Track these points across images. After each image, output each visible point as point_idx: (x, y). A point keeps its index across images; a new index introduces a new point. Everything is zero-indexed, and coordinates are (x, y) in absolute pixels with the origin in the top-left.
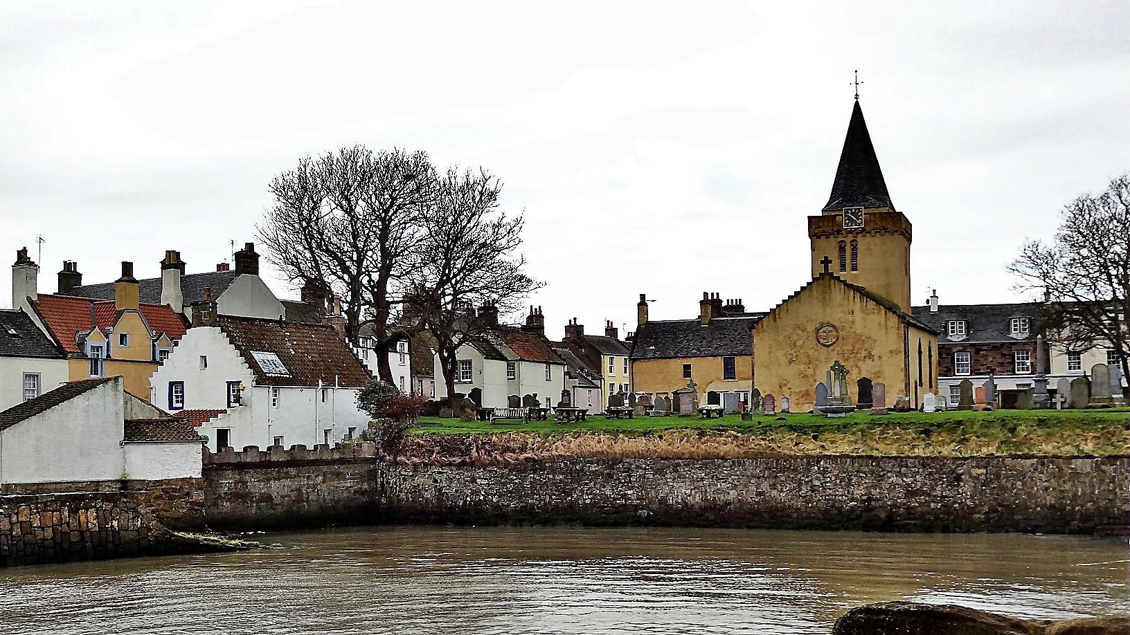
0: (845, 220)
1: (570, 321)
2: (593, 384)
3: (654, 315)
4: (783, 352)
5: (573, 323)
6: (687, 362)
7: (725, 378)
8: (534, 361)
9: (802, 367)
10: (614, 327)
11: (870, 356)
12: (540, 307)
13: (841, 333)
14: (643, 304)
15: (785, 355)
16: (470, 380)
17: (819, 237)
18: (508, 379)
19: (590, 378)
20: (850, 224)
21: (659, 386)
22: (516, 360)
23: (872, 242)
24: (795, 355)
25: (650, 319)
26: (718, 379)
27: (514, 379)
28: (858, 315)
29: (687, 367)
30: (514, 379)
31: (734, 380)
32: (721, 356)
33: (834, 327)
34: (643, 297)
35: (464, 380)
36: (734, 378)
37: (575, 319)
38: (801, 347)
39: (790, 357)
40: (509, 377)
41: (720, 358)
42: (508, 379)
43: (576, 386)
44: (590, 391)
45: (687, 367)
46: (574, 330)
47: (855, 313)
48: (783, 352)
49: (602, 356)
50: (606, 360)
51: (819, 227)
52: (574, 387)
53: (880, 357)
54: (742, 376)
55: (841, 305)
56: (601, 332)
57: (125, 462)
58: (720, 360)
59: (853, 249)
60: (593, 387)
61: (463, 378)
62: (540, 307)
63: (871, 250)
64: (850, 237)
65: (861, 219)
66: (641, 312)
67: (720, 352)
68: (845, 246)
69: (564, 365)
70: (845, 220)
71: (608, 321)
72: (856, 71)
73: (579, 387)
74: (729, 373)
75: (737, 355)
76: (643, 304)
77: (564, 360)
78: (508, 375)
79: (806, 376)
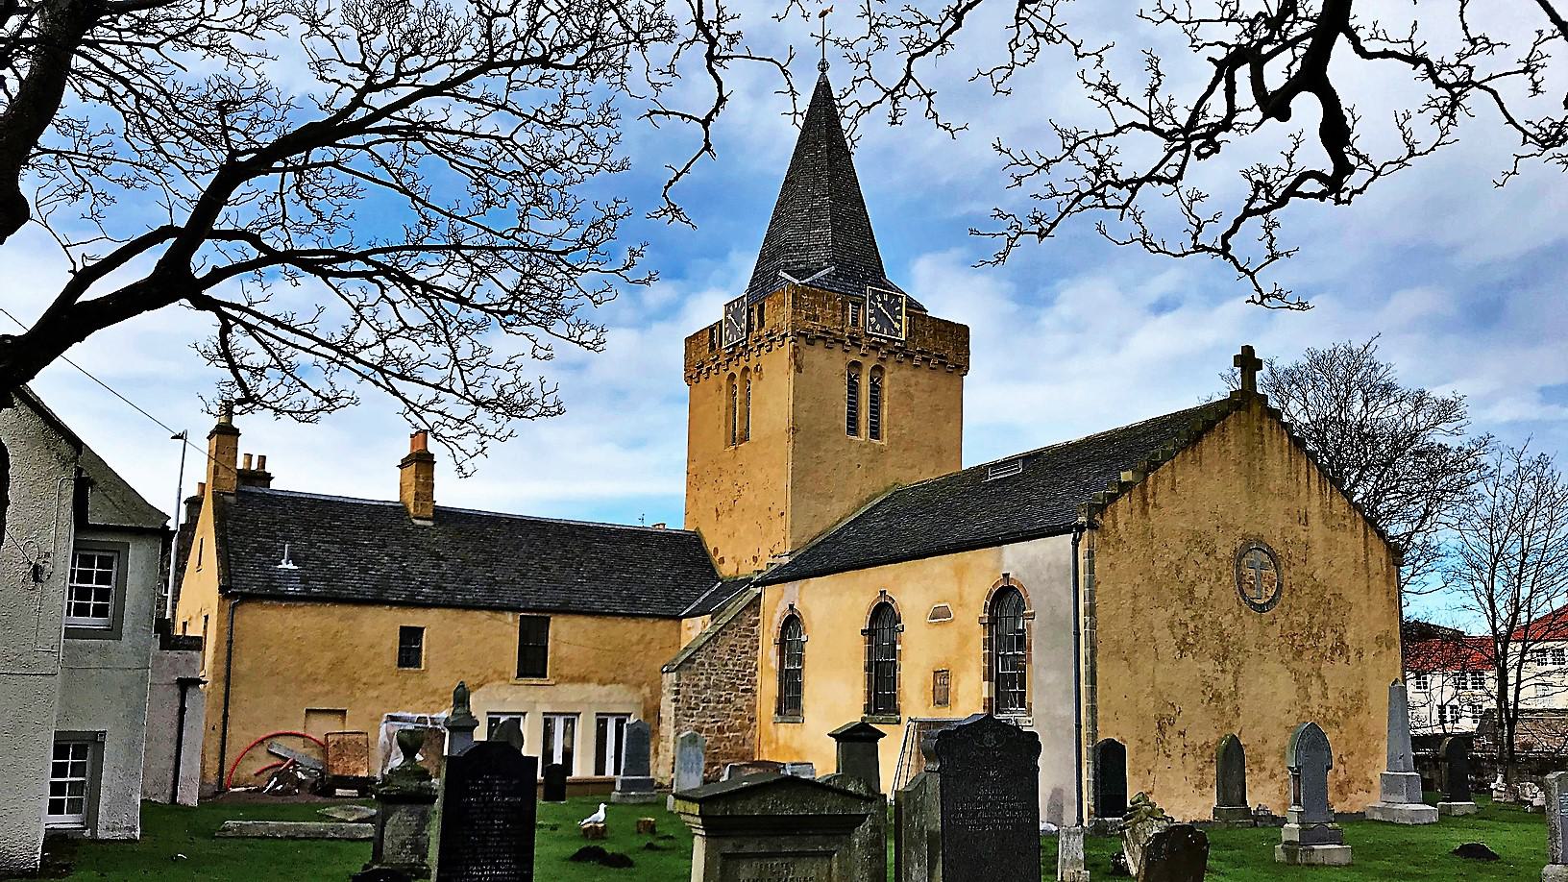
6: (413, 618)
9: (1209, 666)
10: (267, 470)
11: (1341, 647)
13: (1287, 574)
17: (811, 342)
23: (913, 381)
26: (502, 676)
28: (1317, 530)
29: (410, 638)
32: (514, 610)
33: (1272, 556)
39: (1180, 632)
41: (509, 617)
45: (410, 638)
47: (1310, 521)
51: (815, 318)
53: (1360, 653)
54: (566, 671)
55: (1283, 494)
57: (716, 110)
63: (911, 397)
66: (95, 458)
67: (509, 596)
72: (812, 35)
74: (532, 662)
75: (557, 612)
79: (1217, 697)
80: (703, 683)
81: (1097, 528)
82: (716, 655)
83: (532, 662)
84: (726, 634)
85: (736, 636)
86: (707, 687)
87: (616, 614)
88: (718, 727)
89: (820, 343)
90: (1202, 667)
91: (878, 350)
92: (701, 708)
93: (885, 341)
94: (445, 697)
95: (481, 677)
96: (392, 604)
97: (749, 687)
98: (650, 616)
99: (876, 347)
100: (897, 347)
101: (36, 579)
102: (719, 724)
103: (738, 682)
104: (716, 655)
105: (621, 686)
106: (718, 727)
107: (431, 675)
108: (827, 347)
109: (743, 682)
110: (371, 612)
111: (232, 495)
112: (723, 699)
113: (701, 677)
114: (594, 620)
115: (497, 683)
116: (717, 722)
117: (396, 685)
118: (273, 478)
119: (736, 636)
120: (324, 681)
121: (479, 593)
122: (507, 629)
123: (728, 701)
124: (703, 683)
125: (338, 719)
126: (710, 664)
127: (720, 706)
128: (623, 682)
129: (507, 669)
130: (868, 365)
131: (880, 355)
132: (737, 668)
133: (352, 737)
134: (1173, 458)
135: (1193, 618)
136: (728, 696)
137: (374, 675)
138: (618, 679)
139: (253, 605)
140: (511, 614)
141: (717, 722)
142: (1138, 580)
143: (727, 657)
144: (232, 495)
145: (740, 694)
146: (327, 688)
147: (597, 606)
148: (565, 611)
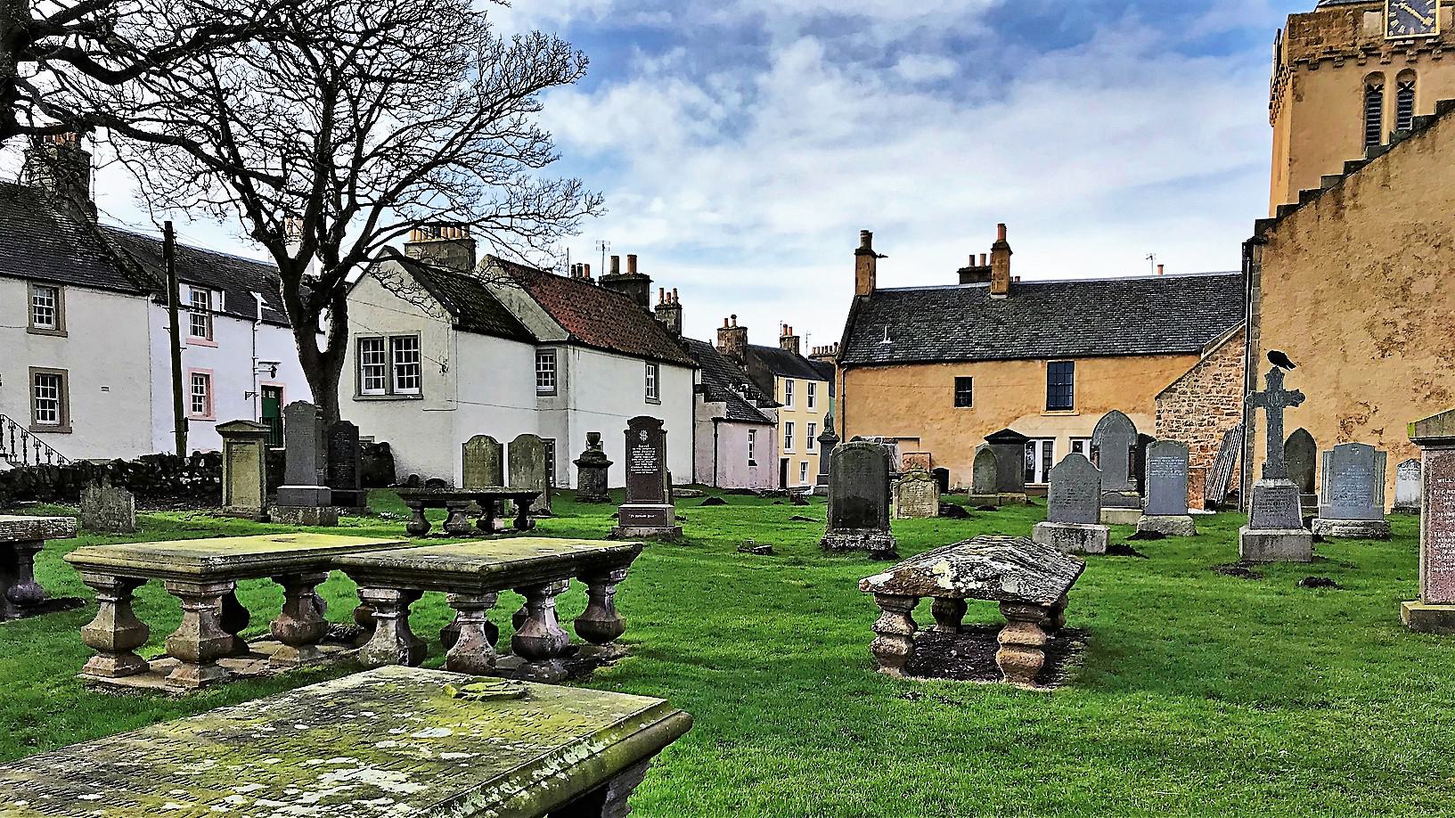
0: (1390, 20)
1: (726, 320)
2: (759, 415)
3: (888, 277)
4: (1360, 316)
5: (730, 324)
6: (963, 371)
7: (1048, 408)
8: (611, 350)
12: (675, 290)
14: (866, 254)
15: (1370, 327)
16: (415, 390)
17: (1314, 67)
18: (539, 394)
19: (754, 403)
20: (1402, 30)
21: (901, 424)
22: (559, 343)
24: (1403, 324)
25: (878, 286)
26: (1033, 409)
27: (554, 393)
29: (963, 385)
30: (554, 393)
31: (1069, 412)
34: (867, 237)
35: (406, 391)
36: (1071, 408)
37: (734, 317)
38: (1428, 298)
39: (1382, 333)
40: (37, 325)
42: (539, 394)
43: (721, 420)
44: (754, 431)
45: (963, 385)
46: (736, 333)
48: (1360, 316)
49: (776, 378)
50: (781, 382)
52: (716, 420)
56: (773, 342)
58: (1039, 370)
59: (1400, 96)
60: (759, 423)
61: (401, 385)
62: (675, 290)
64: (1399, 64)
65: (1432, 16)
67: (1041, 350)
68: (1381, 87)
69: (694, 368)
70: (1390, 20)
71: (786, 326)
73: (729, 421)
74: (1059, 398)
75: (1079, 357)
76: (866, 254)
77: (696, 357)
78: (539, 383)
80: (1185, 409)
81: (1266, 243)
82: (1199, 383)
83: (1059, 398)
84: (1209, 365)
85: (1220, 365)
86: (1188, 412)
87: (1134, 355)
88: (1201, 446)
89: (1326, 66)
90: (1417, 364)
91: (1405, 53)
92: (1183, 431)
93: (1412, 42)
94: (989, 427)
95: (1017, 412)
96: (948, 362)
97: (1235, 411)
98: (1168, 354)
99: (1401, 51)
100: (1428, 44)
101: (444, 371)
102: (1202, 444)
103: (1223, 407)
104: (1199, 383)
105: (1140, 414)
106: (1201, 446)
107: (979, 410)
108: (1336, 67)
109: (1228, 407)
110: (932, 369)
111: (866, 296)
112: (1206, 422)
113: (1183, 404)
114: (1114, 360)
115: (1030, 415)
116: (1200, 442)
117: (952, 420)
118: (1243, 244)
119: (1220, 365)
120: (904, 419)
121: (1019, 347)
122: (1038, 372)
123: (1213, 424)
124: (1185, 409)
125: (914, 444)
126: (1192, 393)
127: (1203, 428)
128: (1144, 412)
129: (1038, 405)
130: (1391, 74)
131: (1408, 59)
132: (1221, 394)
133: (920, 455)
134: (1388, 152)
135: (1406, 316)
136: (1212, 420)
137: (937, 414)
138: (1138, 408)
139: (858, 371)
140: (1040, 361)
141: (1200, 442)
142: (1323, 285)
143: (1210, 385)
144: (866, 296)
145: (1225, 417)
146: (905, 423)
147: (1120, 348)
148: (1088, 355)
